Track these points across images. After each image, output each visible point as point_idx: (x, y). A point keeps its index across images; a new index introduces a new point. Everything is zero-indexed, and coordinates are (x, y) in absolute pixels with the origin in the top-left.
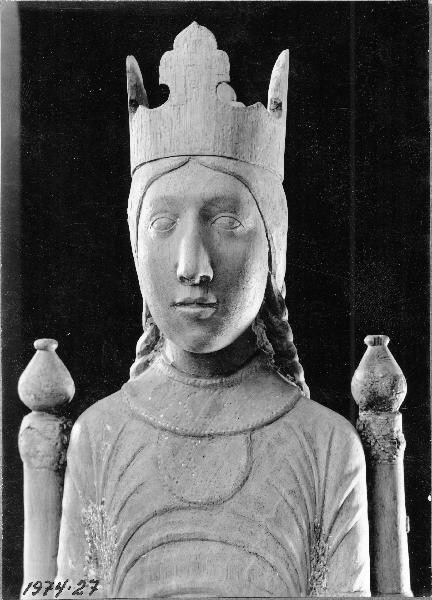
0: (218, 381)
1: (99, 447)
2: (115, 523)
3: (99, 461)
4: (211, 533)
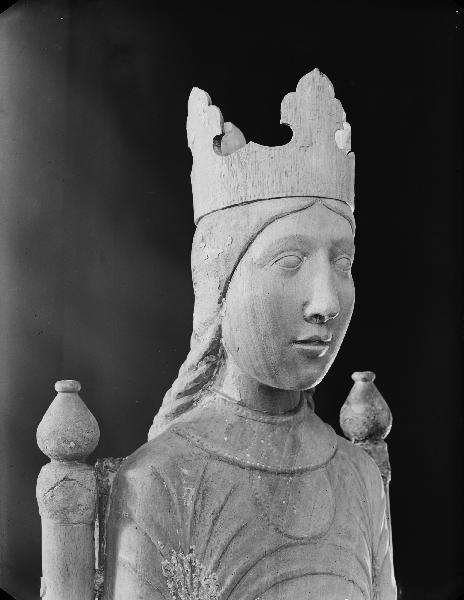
0: (292, 418)
1: (179, 493)
2: (215, 569)
3: (183, 508)
4: (319, 568)
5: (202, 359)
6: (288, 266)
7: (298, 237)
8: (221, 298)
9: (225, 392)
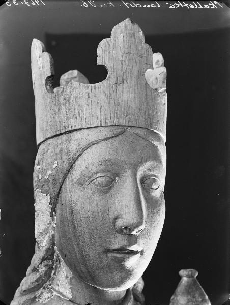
5: (41, 263)
6: (101, 185)
7: (110, 160)
8: (52, 212)
9: (61, 290)
